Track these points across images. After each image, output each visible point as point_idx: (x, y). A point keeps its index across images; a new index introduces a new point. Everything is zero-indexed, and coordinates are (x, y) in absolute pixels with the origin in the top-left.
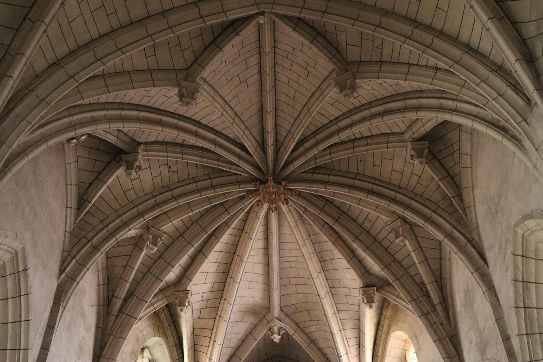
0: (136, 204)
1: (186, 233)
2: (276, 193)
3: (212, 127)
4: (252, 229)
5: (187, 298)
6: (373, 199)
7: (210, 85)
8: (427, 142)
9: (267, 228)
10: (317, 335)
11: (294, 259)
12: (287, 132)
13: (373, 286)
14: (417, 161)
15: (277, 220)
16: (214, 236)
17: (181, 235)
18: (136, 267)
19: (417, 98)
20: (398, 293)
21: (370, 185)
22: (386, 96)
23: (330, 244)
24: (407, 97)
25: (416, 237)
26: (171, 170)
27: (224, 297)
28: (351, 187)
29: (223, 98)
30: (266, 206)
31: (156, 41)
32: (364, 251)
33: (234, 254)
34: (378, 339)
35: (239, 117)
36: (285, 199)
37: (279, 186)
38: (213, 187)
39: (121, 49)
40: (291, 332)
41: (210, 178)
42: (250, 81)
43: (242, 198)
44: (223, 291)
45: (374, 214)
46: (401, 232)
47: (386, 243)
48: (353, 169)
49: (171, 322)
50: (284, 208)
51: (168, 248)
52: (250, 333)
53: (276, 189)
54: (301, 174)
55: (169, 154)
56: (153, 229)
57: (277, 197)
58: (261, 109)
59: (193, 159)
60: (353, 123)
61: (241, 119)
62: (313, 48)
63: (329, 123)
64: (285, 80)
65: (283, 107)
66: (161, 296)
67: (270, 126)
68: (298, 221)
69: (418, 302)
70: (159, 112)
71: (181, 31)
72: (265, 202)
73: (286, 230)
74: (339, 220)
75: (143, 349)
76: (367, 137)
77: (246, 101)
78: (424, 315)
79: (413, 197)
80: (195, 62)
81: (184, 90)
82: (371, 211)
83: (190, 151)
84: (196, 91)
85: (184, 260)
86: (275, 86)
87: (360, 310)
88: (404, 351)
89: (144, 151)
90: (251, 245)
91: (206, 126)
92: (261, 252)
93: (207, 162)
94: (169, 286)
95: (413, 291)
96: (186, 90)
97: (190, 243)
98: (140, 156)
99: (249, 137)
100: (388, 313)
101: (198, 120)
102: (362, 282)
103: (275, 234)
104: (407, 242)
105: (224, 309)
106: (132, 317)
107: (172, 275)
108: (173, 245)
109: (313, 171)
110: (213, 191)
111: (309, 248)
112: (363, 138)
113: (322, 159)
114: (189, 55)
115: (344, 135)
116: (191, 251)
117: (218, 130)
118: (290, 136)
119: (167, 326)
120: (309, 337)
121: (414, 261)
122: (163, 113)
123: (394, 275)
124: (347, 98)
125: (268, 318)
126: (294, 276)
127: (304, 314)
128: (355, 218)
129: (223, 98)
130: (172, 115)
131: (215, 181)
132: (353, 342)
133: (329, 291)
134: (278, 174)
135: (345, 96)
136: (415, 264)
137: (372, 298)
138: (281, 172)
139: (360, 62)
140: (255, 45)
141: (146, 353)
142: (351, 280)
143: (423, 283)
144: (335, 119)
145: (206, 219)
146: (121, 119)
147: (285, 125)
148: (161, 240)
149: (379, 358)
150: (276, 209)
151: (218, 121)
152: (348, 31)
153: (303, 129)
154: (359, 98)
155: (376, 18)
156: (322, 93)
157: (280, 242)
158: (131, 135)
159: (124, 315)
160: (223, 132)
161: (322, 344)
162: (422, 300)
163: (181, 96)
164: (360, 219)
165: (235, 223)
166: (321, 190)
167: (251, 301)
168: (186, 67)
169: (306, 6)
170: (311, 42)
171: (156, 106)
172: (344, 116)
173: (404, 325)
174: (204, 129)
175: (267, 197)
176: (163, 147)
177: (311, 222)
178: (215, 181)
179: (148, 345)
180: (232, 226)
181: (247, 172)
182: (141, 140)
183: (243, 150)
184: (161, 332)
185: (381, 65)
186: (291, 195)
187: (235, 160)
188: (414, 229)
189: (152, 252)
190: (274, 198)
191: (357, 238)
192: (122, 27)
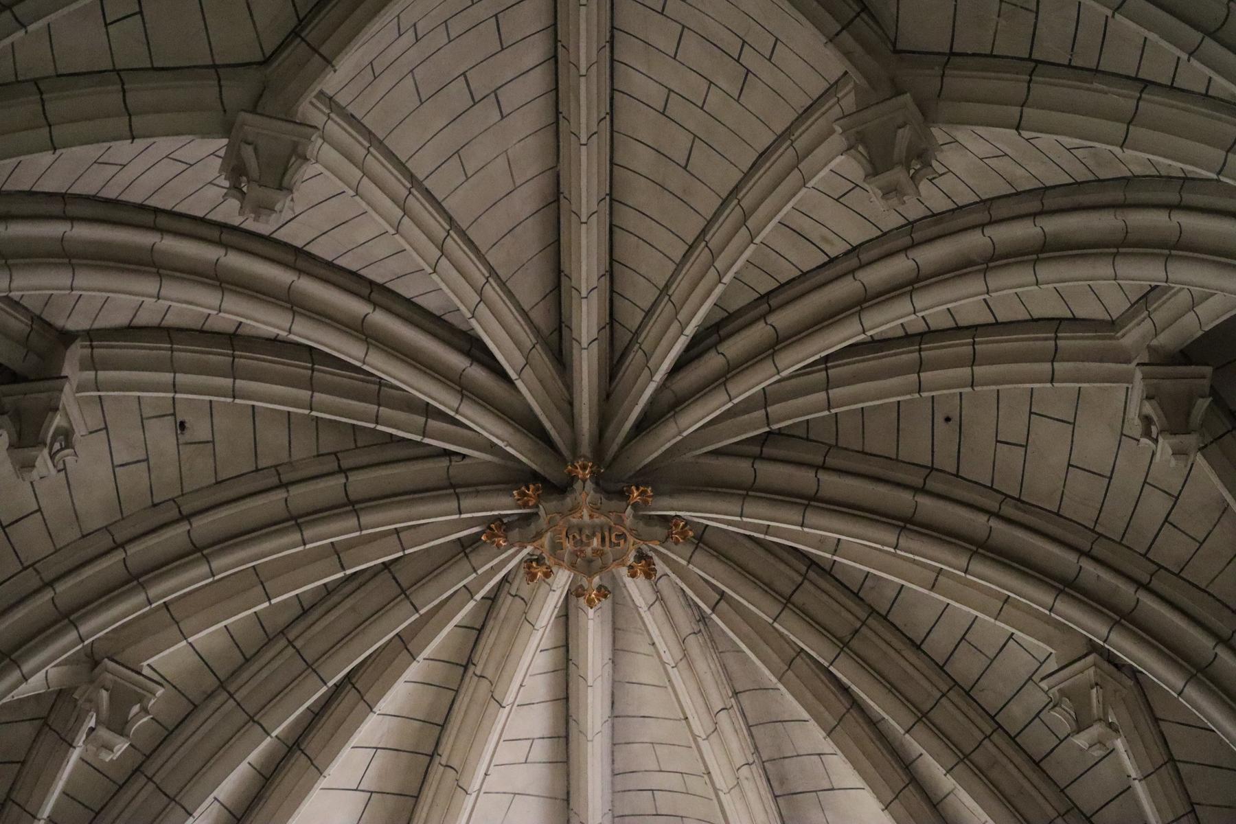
0: (48, 576)
1: (245, 675)
2: (602, 531)
3: (354, 268)
4: (506, 659)
7: (351, 119)
8: (1208, 370)
9: (568, 660)
11: (674, 782)
14: (1165, 446)
16: (356, 690)
17: (222, 685)
19: (1170, 207)
21: (982, 519)
24: (1132, 196)
25: (1156, 720)
26: (187, 437)
28: (906, 523)
30: (563, 578)
33: (432, 756)
35: (463, 234)
36: (641, 556)
37: (614, 504)
38: (351, 505)
41: (341, 470)
42: (513, 96)
43: (466, 547)
45: (993, 628)
46: (1096, 709)
48: (916, 448)
53: (603, 519)
54: (701, 460)
55: (181, 377)
57: (607, 548)
58: (555, 201)
59: (275, 396)
64: (655, 95)
65: (639, 193)
67: (586, 267)
68: (692, 640)
70: (148, 219)
72: (560, 565)
73: (643, 669)
74: (855, 644)
77: (493, 173)
79: (1145, 578)
80: (295, 33)
81: (248, 152)
83: (266, 362)
84: (297, 154)
86: (611, 113)
89: (83, 368)
90: (499, 727)
91: (330, 265)
92: (541, 751)
96: (256, 150)
98: (67, 396)
101: (299, 243)
103: (598, 683)
104: (1120, 744)
110: (353, 522)
111: (734, 744)
112: (958, 330)
116: (259, 751)
117: (380, 280)
118: (665, 309)
122: (163, 221)
124: (894, 201)
128: (917, 634)
129: (401, 166)
131: (361, 482)
134: (615, 458)
144: (846, 254)
145: (317, 628)
147: (649, 266)
148: (145, 711)
150: (603, 592)
151: (380, 249)
153: (720, 289)
156: (800, 159)
157: (616, 714)
160: (400, 288)
163: (236, 171)
164: (939, 643)
171: (135, 196)
174: (326, 281)
175: (569, 546)
176: (161, 351)
177: (743, 647)
178: (361, 482)
181: (492, 448)
182: (71, 325)
183: (474, 359)
186: (662, 543)
187: (444, 399)
189: (108, 757)
190: (595, 551)
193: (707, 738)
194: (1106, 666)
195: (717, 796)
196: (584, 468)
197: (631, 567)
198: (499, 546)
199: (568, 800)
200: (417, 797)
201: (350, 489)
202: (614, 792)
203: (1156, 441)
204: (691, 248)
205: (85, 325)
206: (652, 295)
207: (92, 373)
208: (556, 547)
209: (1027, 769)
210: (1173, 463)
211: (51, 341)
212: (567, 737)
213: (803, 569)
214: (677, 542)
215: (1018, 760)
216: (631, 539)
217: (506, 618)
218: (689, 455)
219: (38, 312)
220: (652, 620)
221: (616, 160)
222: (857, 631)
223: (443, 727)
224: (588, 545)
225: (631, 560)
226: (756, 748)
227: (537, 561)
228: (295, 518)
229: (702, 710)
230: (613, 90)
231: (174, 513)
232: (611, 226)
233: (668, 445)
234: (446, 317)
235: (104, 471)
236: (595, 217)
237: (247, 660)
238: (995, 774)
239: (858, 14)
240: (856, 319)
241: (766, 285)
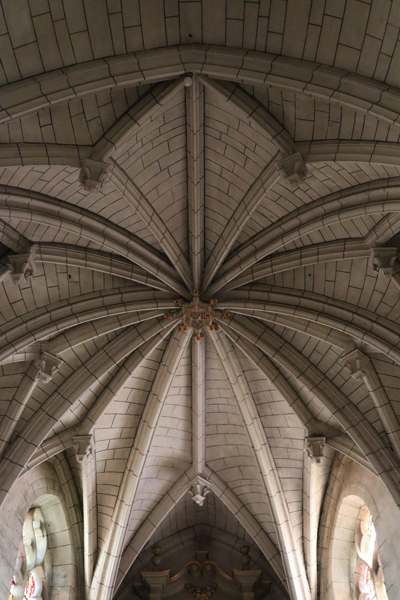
2: (202, 315)
3: (124, 227)
4: (171, 363)
5: (89, 444)
6: (323, 321)
7: (122, 169)
9: (191, 361)
10: (250, 498)
11: (224, 401)
12: (218, 237)
13: (321, 435)
14: (382, 271)
15: (204, 352)
17: (83, 364)
18: (25, 402)
19: (384, 188)
20: (351, 445)
21: (321, 304)
22: (343, 188)
23: (269, 381)
25: (377, 373)
26: (71, 280)
27: (135, 446)
28: (297, 307)
29: (138, 189)
30: (190, 331)
31: (52, 103)
32: (311, 390)
33: (149, 392)
34: (326, 504)
36: (213, 323)
38: (123, 304)
39: (5, 109)
40: (218, 493)
41: (120, 293)
43: (160, 320)
44: (134, 438)
45: (325, 343)
47: (339, 381)
48: (300, 284)
49: (69, 477)
50: (212, 334)
51: (65, 380)
52: (167, 492)
54: (234, 292)
55: (69, 259)
56: (46, 353)
57: (203, 320)
58: (187, 207)
59: (99, 267)
60: (300, 225)
61: (160, 219)
62: (253, 121)
63: (271, 225)
65: (213, 205)
66: (57, 440)
67: (197, 229)
68: (230, 353)
69: (378, 455)
71: (84, 92)
73: (215, 364)
75: (32, 510)
76: (318, 244)
77: (168, 194)
78: (386, 472)
79: (375, 319)
80: (103, 136)
82: (322, 340)
84: (103, 171)
85: (85, 396)
86: (204, 176)
87: (304, 467)
88: (358, 521)
89: (37, 253)
92: (183, 391)
93: (117, 272)
94: (66, 429)
95: (372, 441)
96: (90, 169)
97: (93, 375)
99: (170, 241)
100: (339, 473)
101: (106, 217)
102: (307, 431)
103: (201, 368)
104: (365, 379)
105: (135, 461)
106: (18, 465)
107: (70, 415)
108: (73, 377)
109: (249, 288)
110: (124, 308)
111: (243, 387)
112: (313, 245)
113: (261, 272)
114: (95, 128)
115: (289, 241)
116: (95, 385)
117: (132, 232)
119: (65, 481)
120: (240, 500)
121: (373, 403)
122: (62, 204)
123: (348, 420)
125: (190, 474)
126: (223, 423)
127: (234, 470)
129: (138, 189)
130: (72, 208)
131: (126, 297)
132: (294, 507)
133: (266, 442)
134: (206, 292)
135: (292, 182)
136: (375, 407)
137: (320, 450)
138: (211, 287)
139: (313, 141)
140: (181, 122)
141: (37, 514)
142: (294, 427)
143: (384, 431)
146: (7, 205)
147: (216, 228)
148: (57, 368)
149: (326, 529)
150: (202, 335)
151: (133, 220)
152: (297, 98)
154: (310, 192)
155: (335, 79)
158: (20, 230)
159: (8, 461)
161: (256, 509)
162: (384, 453)
163: (83, 179)
164: (307, 351)
165: (151, 353)
166: (257, 311)
167: (169, 453)
168: (92, 144)
169: (244, 66)
170: (250, 115)
171: (53, 194)
172: (289, 216)
173: (359, 487)
175: (191, 319)
176: (63, 250)
178: (126, 297)
179: (40, 505)
180: (148, 356)
181: (167, 288)
182: (34, 239)
184: (57, 488)
185: (339, 144)
187: (152, 271)
188: (376, 366)
190: (200, 321)
191: (302, 374)
192: (9, 84)
193: (235, 384)
194: (361, 353)
195: (238, 404)
196: (196, 292)
197: (211, 326)
198: (170, 319)
199: (192, 407)
200: (145, 405)
201: (123, 299)
202: (206, 405)
203: (378, 271)
204: (229, 221)
205: (38, 240)
206: (217, 238)
207: (40, 255)
208: (187, 319)
209: (335, 390)
210: (384, 277)
211: (26, 244)
212: (191, 387)
213: (264, 328)
214: (225, 318)
215: (333, 387)
216: (211, 316)
217: (172, 346)
218: (229, 290)
219: (22, 234)
220: (217, 346)
221: (206, 194)
222: (281, 347)
223: (153, 382)
224: (198, 318)
225: (211, 324)
226: (250, 389)
227: (182, 325)
228: (106, 307)
229: (233, 375)
230: (205, 169)
231: (67, 303)
232: (204, 216)
233: (222, 286)
234: (153, 246)
235: (44, 289)
236: (199, 211)
237: (91, 357)
238: (325, 392)
239: (282, 130)
240: (281, 240)
241: (253, 234)
